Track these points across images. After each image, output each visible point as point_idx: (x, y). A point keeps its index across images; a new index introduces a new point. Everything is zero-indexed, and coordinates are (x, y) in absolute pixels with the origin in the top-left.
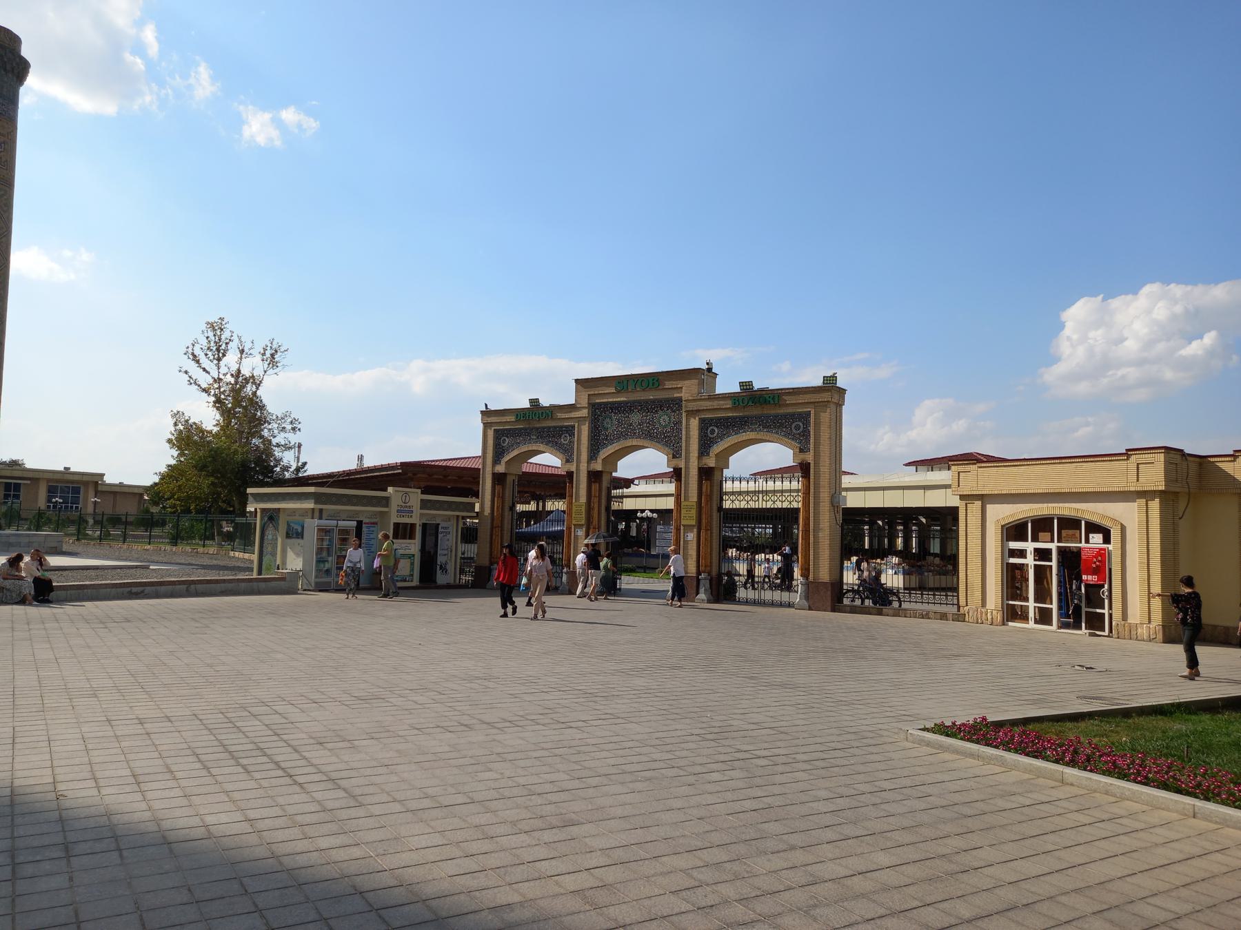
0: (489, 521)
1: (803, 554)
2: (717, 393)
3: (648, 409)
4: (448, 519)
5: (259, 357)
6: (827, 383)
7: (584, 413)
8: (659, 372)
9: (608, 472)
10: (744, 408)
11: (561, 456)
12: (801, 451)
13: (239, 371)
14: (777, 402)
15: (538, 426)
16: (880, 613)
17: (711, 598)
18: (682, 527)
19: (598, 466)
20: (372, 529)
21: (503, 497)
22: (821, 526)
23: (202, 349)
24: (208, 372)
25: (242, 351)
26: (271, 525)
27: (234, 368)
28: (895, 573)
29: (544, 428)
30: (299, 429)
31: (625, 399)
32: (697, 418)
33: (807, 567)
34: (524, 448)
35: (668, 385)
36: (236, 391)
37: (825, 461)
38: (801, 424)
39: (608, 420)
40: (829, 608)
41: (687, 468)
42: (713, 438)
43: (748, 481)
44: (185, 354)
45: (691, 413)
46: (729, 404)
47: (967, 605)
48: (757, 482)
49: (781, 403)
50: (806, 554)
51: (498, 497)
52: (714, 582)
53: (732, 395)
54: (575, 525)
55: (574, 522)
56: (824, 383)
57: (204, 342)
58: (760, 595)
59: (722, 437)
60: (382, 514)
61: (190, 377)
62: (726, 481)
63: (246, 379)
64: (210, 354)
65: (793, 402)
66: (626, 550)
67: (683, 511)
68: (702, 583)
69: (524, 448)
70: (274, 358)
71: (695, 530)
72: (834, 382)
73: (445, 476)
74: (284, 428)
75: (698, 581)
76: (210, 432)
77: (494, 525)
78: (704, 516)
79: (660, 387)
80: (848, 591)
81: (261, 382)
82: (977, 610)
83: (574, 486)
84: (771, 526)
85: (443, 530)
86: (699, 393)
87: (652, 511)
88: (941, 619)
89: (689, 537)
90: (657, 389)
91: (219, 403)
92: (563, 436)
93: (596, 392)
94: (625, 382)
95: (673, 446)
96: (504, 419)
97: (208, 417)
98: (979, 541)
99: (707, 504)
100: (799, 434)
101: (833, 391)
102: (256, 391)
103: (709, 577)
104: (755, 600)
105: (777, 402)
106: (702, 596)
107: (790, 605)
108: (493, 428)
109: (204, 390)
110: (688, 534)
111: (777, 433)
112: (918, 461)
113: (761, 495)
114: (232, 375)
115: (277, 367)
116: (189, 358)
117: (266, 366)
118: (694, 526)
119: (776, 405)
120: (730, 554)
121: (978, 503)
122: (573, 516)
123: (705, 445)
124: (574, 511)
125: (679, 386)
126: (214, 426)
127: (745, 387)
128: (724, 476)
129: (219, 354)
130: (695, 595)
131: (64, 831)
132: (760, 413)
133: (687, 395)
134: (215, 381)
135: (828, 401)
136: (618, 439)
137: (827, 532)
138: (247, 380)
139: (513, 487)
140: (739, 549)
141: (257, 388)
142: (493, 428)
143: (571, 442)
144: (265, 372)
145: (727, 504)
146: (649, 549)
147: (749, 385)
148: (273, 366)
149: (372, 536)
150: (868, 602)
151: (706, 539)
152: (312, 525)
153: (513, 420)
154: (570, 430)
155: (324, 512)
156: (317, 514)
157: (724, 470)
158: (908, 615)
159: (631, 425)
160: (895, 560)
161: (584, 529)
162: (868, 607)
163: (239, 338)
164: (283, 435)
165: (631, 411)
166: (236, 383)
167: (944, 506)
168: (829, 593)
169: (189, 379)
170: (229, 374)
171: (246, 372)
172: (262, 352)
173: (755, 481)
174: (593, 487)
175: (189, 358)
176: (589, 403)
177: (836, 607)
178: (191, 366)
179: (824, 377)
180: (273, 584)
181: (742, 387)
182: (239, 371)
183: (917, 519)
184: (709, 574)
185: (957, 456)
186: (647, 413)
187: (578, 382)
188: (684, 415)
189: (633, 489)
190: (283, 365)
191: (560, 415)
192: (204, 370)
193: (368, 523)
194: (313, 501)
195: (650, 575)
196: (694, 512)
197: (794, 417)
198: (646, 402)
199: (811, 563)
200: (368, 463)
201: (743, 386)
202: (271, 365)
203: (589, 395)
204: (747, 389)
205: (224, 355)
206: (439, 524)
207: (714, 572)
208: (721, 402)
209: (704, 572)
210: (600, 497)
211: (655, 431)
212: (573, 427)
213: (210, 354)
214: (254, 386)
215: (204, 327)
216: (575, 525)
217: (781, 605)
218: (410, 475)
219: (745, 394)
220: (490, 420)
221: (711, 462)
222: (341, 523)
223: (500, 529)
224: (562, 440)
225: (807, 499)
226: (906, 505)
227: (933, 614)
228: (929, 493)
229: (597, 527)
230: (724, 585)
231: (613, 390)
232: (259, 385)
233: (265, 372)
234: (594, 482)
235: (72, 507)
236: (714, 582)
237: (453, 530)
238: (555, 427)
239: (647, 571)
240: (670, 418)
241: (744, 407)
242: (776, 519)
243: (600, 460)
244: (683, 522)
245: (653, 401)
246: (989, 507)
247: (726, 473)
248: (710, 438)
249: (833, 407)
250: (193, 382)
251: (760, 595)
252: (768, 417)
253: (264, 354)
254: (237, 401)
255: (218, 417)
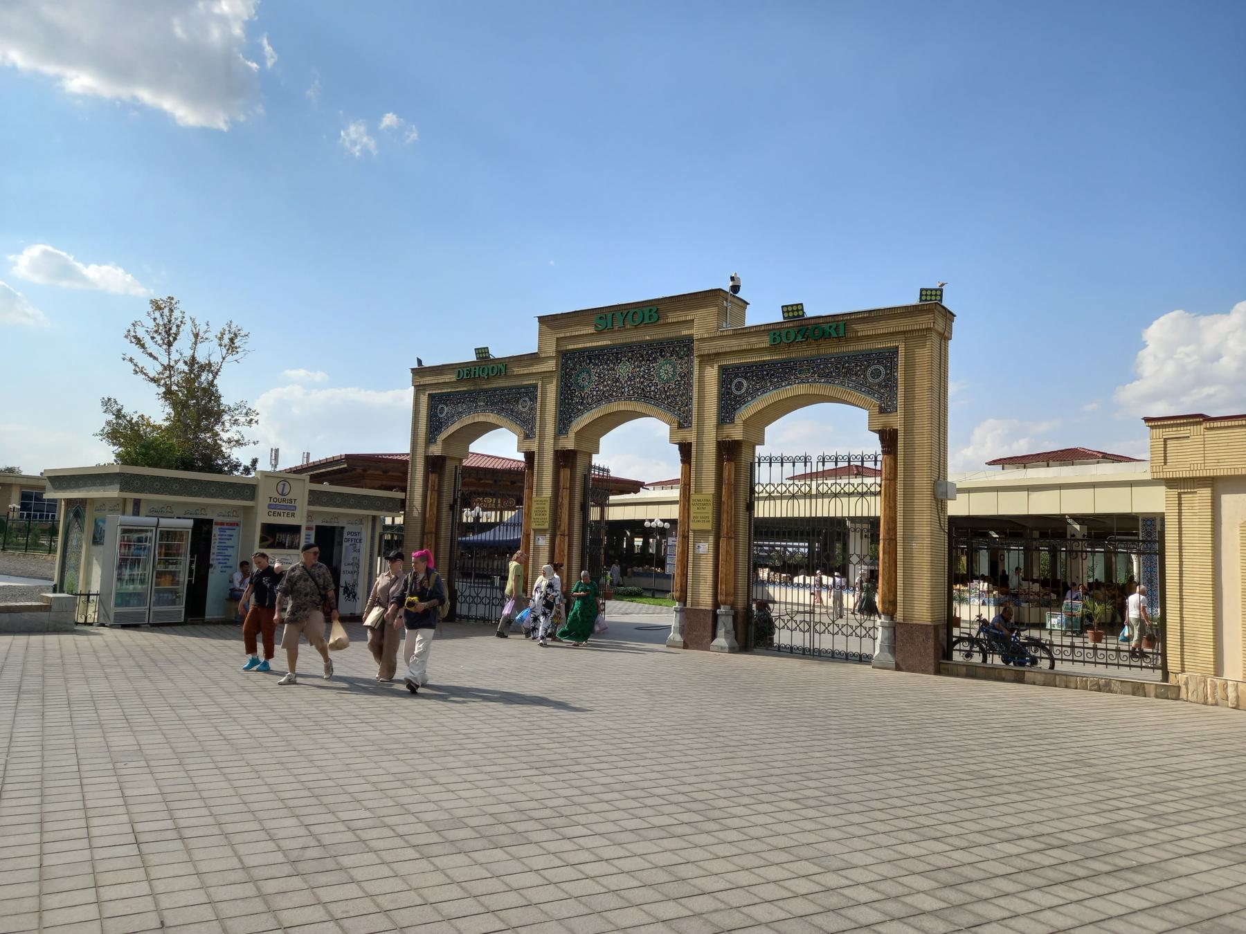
0: (419, 525)
1: (886, 578)
2: (747, 325)
3: (642, 356)
4: (360, 520)
5: (216, 341)
6: (926, 300)
7: (551, 365)
8: (659, 300)
9: (585, 453)
10: (789, 346)
11: (518, 429)
12: (882, 411)
13: (193, 358)
14: (841, 333)
15: (485, 387)
16: (1020, 679)
17: (736, 644)
18: (691, 534)
19: (569, 443)
20: (228, 532)
21: (440, 492)
22: (917, 532)
23: (147, 331)
24: (155, 358)
25: (196, 336)
26: (76, 525)
27: (188, 354)
28: (984, 604)
29: (495, 390)
30: (256, 422)
31: (609, 343)
32: (716, 366)
33: (891, 598)
34: (468, 420)
35: (672, 317)
36: (190, 381)
37: (923, 424)
38: (882, 368)
39: (584, 375)
40: (932, 668)
41: (700, 442)
42: (740, 396)
43: (794, 463)
44: (126, 337)
45: (707, 359)
46: (765, 342)
47: (1183, 671)
48: (809, 464)
49: (849, 335)
50: (890, 578)
51: (433, 490)
52: (740, 619)
53: (771, 327)
54: (534, 530)
55: (534, 526)
56: (921, 300)
57: (151, 325)
58: (812, 640)
59: (753, 394)
60: (247, 510)
61: (136, 365)
62: (759, 463)
63: (202, 366)
64: (158, 338)
65: (870, 333)
66: (635, 569)
67: (693, 509)
68: (721, 620)
69: (468, 420)
70: (233, 343)
71: (711, 539)
72: (938, 298)
73: (385, 472)
74: (236, 420)
75: (715, 617)
76: (160, 427)
77: (426, 531)
78: (724, 516)
79: (661, 322)
80: (960, 640)
81: (218, 370)
82: (1205, 682)
83: (535, 472)
84: (807, 544)
85: (349, 536)
86: (718, 328)
87: (664, 521)
88: (1134, 694)
89: (701, 550)
90: (655, 324)
91: (168, 394)
92: (521, 400)
93: (568, 335)
94: (609, 316)
95: (679, 410)
96: (442, 379)
97: (157, 412)
98: (1209, 560)
99: (729, 497)
100: (879, 384)
101: (936, 313)
102: (213, 381)
103: (732, 612)
104: (810, 649)
105: (841, 333)
106: (721, 641)
107: (862, 659)
108: (427, 393)
109: (153, 380)
110: (701, 545)
111: (842, 384)
112: (1005, 459)
113: (814, 492)
114: (185, 363)
115: (237, 352)
116: (131, 342)
117: (224, 351)
118: (708, 532)
119: (838, 338)
120: (761, 575)
121: (1206, 493)
122: (533, 516)
123: (728, 407)
124: (534, 509)
125: (689, 318)
126: (164, 420)
127: (791, 314)
128: (757, 455)
129: (169, 336)
130: (709, 639)
131: (91, 848)
132: (814, 353)
133: (701, 331)
134: (165, 368)
135: (928, 329)
136: (599, 402)
137: (927, 541)
138: (202, 368)
139: (455, 478)
140: (774, 569)
141: (215, 377)
142: (427, 393)
143: (532, 409)
144: (224, 358)
145: (763, 510)
146: (663, 568)
147: (798, 310)
148: (233, 351)
149: (228, 543)
150: (997, 660)
151: (727, 551)
152: (115, 523)
153: (454, 380)
154: (530, 392)
155: (143, 505)
156: (130, 508)
157: (757, 447)
158: (1073, 685)
159: (617, 380)
160: (984, 586)
161: (548, 536)
162: (994, 668)
163: (193, 321)
164: (235, 428)
165: (618, 360)
166: (191, 371)
167: (1091, 511)
168: (931, 643)
169: (133, 367)
170: (182, 362)
171: (201, 358)
172: (219, 335)
173: (805, 462)
174: (562, 474)
175: (131, 342)
176: (558, 351)
177: (942, 666)
178: (135, 351)
179: (922, 290)
180: (26, 616)
181: (786, 315)
182: (193, 358)
183: (987, 535)
184: (733, 606)
185: (1057, 452)
186: (641, 362)
187: (543, 320)
188: (696, 361)
189: (643, 495)
190: (244, 350)
191: (517, 371)
192: (151, 355)
193: (222, 524)
194: (118, 486)
195: (659, 601)
196: (709, 511)
197: (868, 358)
198: (640, 345)
199: (900, 592)
200: (314, 459)
201: (788, 312)
202: (230, 351)
203: (557, 338)
204: (794, 317)
205: (175, 339)
206: (343, 528)
207: (741, 604)
208: (754, 340)
209: (725, 603)
210: (572, 489)
211: (653, 388)
212: (535, 387)
213: (158, 338)
214: (210, 375)
215: (149, 308)
216: (534, 530)
217: (847, 658)
218: (359, 470)
219: (791, 325)
220: (428, 380)
221: (736, 432)
222: (164, 522)
223: (434, 535)
224: (520, 406)
225: (892, 487)
226: (1001, 513)
227: (1118, 683)
228: (1035, 496)
229: (566, 533)
230: (756, 624)
231: (591, 330)
232: (217, 373)
233: (224, 358)
234: (564, 467)
235: (47, 516)
236: (740, 619)
237: (366, 534)
238: (510, 388)
239: (656, 596)
240: (675, 367)
241: (789, 345)
242: (813, 535)
243: (572, 435)
244: (693, 526)
245: (650, 344)
246: (1228, 500)
247: (760, 451)
248: (736, 396)
249: (935, 338)
250: (139, 371)
251: (812, 640)
252: (826, 360)
253: (221, 339)
254: (191, 393)
255: (169, 410)
